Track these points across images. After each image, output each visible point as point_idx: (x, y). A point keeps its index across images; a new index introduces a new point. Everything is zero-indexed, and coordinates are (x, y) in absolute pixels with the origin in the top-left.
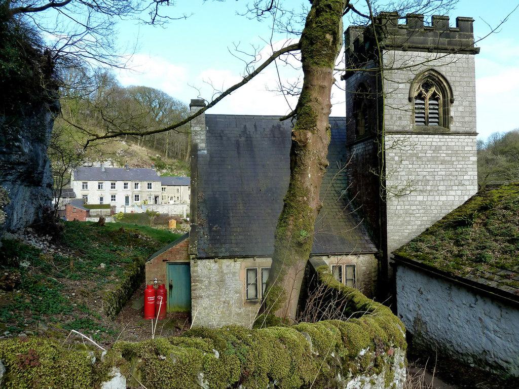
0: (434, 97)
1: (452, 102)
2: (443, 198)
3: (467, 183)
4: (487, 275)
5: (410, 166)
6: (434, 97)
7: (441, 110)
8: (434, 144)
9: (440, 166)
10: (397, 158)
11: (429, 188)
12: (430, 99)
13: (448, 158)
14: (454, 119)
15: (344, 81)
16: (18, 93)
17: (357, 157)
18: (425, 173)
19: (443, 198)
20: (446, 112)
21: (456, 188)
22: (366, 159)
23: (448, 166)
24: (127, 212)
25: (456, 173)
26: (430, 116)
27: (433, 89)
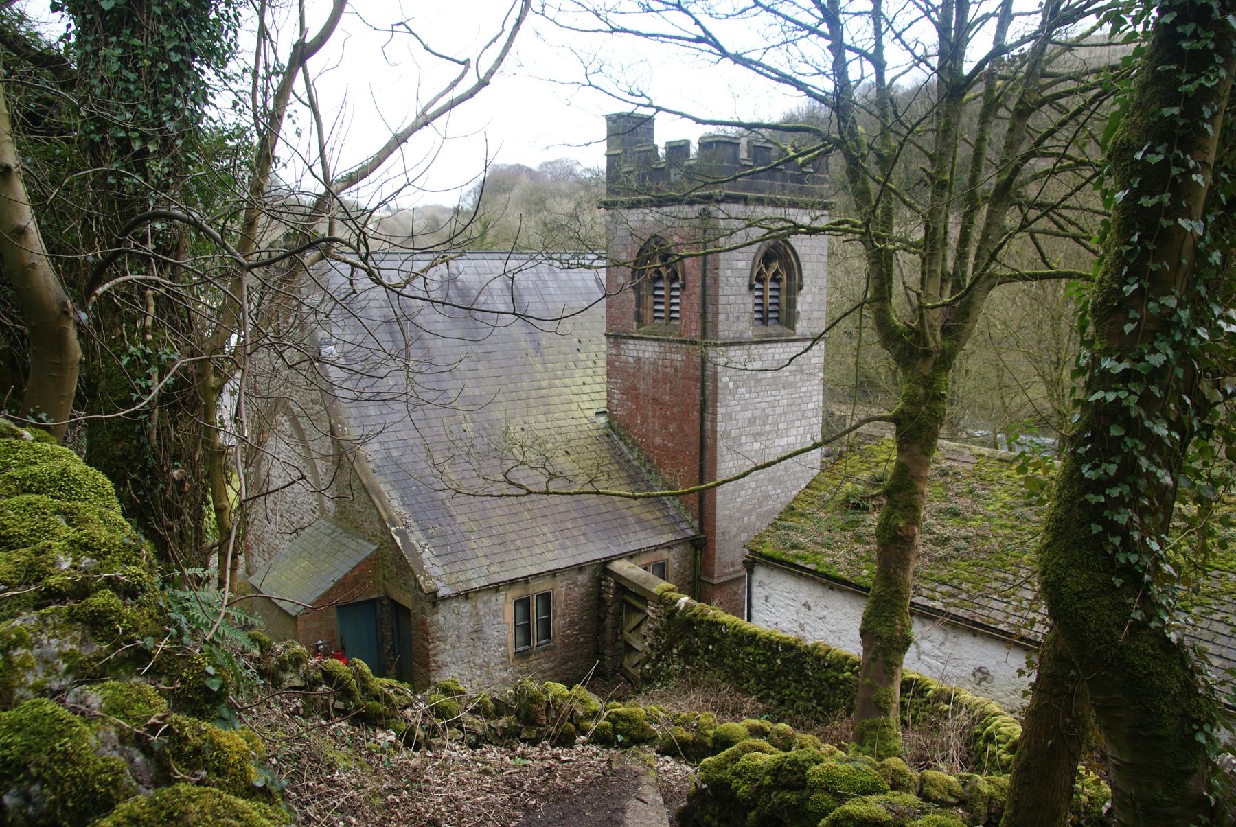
0: (775, 279)
1: (801, 288)
2: (783, 441)
3: (811, 414)
4: (925, 592)
5: (747, 396)
6: (775, 279)
7: (783, 298)
8: (777, 357)
9: (783, 392)
10: (731, 385)
11: (767, 427)
12: (772, 280)
13: (792, 378)
14: (802, 315)
15: (593, 159)
16: (1174, 434)
17: (780, 804)
18: (764, 405)
19: (783, 441)
20: (792, 304)
21: (798, 423)
22: (665, 374)
23: (791, 390)
24: (877, 339)
25: (799, 401)
26: (771, 308)
27: (776, 265)
